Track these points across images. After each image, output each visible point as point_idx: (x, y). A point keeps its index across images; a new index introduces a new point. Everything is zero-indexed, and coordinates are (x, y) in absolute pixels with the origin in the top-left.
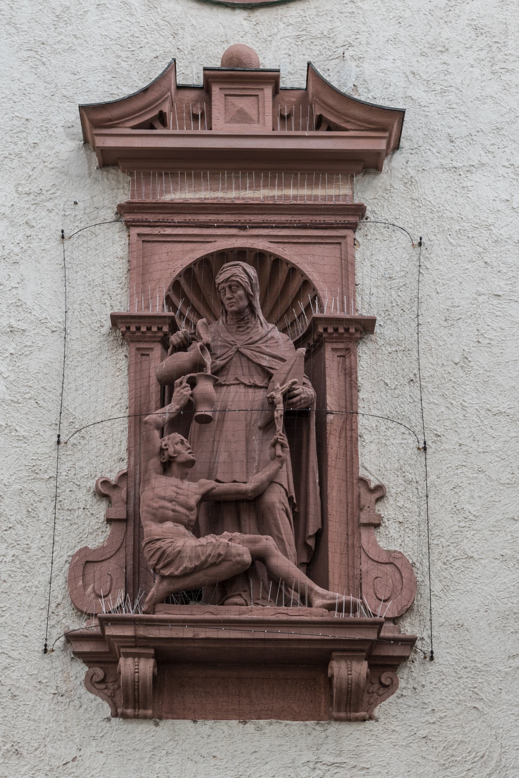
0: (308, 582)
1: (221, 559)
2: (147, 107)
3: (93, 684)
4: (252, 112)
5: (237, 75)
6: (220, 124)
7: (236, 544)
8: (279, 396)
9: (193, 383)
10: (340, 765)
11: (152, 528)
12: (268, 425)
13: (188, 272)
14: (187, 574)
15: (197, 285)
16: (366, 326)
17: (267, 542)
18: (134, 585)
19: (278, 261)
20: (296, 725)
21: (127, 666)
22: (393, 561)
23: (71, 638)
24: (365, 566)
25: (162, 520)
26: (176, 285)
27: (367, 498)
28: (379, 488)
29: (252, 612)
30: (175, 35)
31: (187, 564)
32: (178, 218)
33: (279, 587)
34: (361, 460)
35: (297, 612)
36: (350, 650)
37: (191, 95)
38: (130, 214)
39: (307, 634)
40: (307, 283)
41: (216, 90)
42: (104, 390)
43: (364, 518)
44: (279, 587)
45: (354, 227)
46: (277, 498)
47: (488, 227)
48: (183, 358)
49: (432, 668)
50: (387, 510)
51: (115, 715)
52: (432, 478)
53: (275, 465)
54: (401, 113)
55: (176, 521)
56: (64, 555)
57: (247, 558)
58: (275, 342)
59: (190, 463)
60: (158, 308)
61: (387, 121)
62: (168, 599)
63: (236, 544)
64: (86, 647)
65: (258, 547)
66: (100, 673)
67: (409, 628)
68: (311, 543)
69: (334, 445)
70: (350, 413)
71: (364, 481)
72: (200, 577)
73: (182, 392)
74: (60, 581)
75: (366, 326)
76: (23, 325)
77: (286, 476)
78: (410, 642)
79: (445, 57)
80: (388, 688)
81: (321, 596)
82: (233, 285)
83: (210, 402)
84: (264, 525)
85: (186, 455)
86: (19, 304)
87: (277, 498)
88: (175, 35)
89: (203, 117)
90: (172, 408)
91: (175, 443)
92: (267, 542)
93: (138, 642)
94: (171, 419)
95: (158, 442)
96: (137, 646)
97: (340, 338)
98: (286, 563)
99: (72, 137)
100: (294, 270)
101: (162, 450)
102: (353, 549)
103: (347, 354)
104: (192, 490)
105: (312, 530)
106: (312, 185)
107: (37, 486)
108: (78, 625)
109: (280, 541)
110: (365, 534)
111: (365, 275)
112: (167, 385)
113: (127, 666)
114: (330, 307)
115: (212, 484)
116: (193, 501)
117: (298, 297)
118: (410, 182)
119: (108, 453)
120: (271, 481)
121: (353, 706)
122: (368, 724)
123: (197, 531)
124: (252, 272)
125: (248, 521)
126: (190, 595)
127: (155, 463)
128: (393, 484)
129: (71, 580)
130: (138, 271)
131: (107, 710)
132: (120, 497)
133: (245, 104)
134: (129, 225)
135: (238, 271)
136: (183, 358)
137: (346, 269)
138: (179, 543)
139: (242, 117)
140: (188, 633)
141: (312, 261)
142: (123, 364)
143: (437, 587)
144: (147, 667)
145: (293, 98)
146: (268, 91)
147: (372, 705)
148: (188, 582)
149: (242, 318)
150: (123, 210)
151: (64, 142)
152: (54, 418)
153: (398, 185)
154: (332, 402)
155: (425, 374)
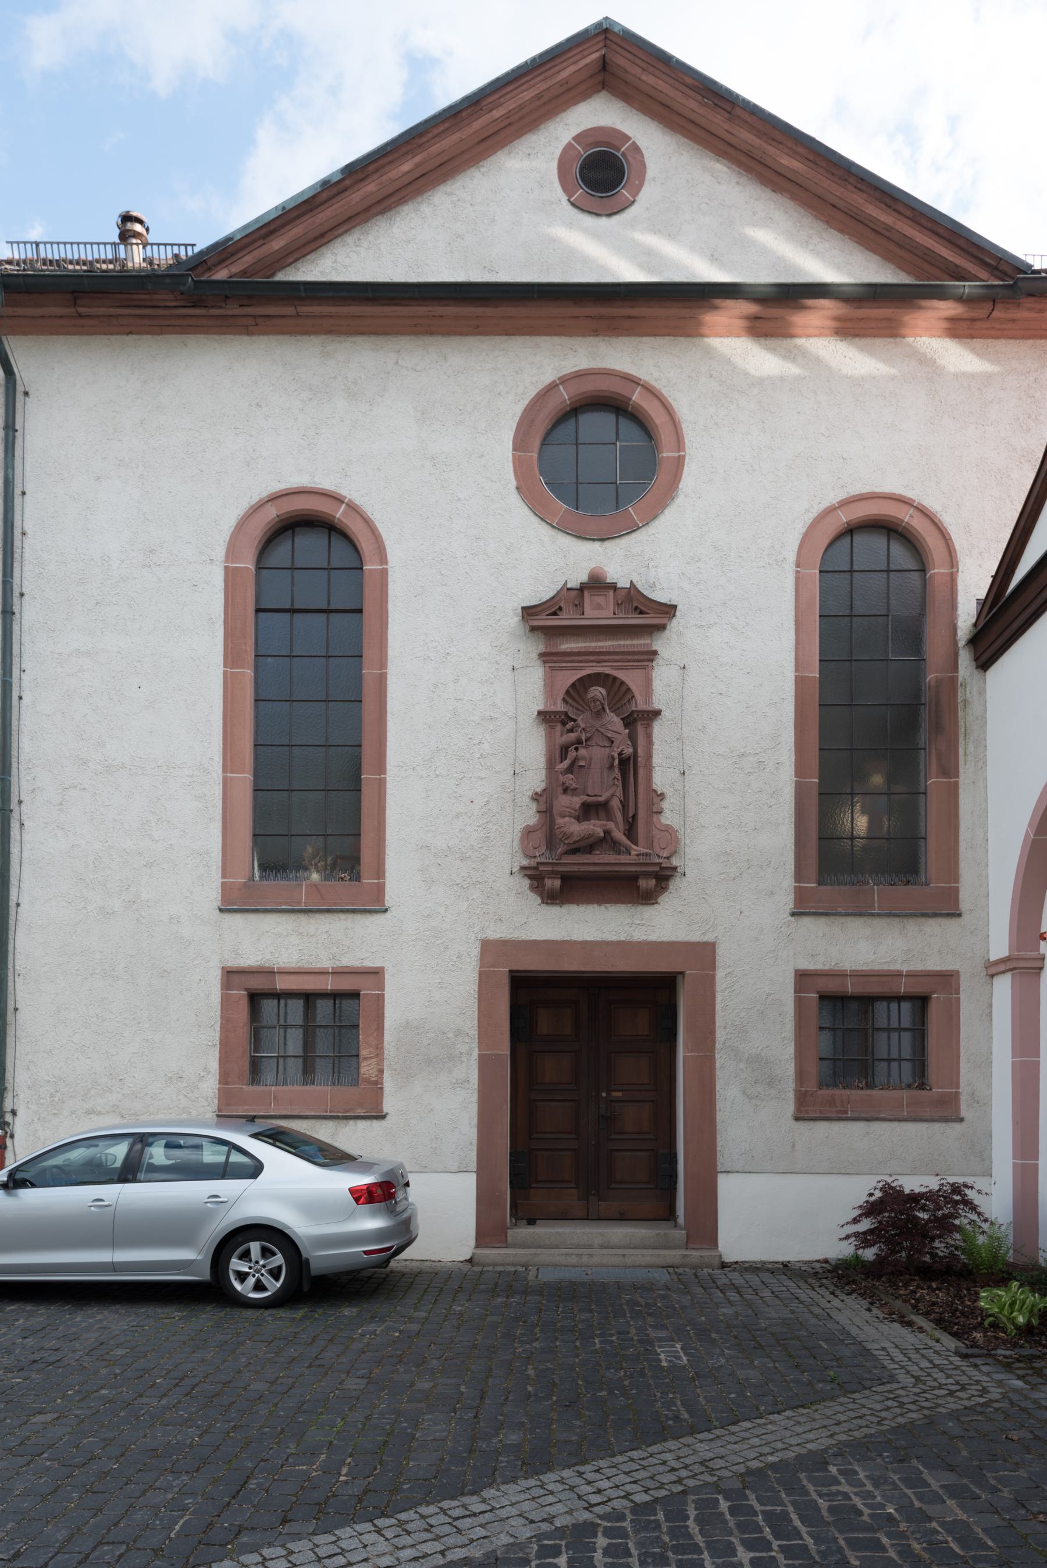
0: (628, 842)
1: (590, 836)
2: (552, 607)
3: (533, 888)
4: (604, 604)
5: (596, 584)
6: (588, 611)
7: (595, 827)
8: (616, 755)
9: (577, 749)
10: (642, 925)
11: (559, 821)
12: (611, 767)
13: (573, 685)
14: (575, 842)
15: (577, 691)
16: (657, 713)
17: (611, 825)
18: (550, 845)
19: (615, 679)
20: (622, 907)
21: (548, 883)
22: (668, 829)
23: (523, 868)
24: (655, 832)
25: (564, 817)
26: (568, 692)
27: (656, 799)
28: (662, 794)
29: (603, 859)
30: (565, 556)
31: (576, 838)
32: (568, 659)
33: (616, 846)
34: (654, 780)
35: (624, 859)
36: (647, 875)
37: (574, 593)
38: (545, 657)
39: (629, 869)
40: (629, 689)
41: (586, 593)
42: (533, 749)
43: (655, 810)
44: (616, 846)
45: (652, 661)
46: (616, 803)
47: (717, 658)
48: (573, 736)
49: (685, 879)
50: (665, 805)
51: (543, 902)
52: (687, 788)
53: (614, 788)
54: (676, 607)
55: (570, 816)
56: (519, 828)
57: (602, 835)
58: (614, 721)
59: (576, 789)
60: (560, 707)
61: (669, 610)
62: (566, 853)
63: (595, 827)
64: (529, 872)
65: (607, 827)
66: (536, 884)
67: (675, 862)
68: (630, 820)
69: (641, 772)
70: (649, 756)
71: (655, 791)
72: (581, 844)
73: (572, 754)
74: (517, 842)
75: (657, 713)
76: (496, 716)
77: (619, 792)
78: (675, 868)
79: (699, 564)
80: (664, 889)
81: (635, 849)
82: (595, 700)
83: (584, 758)
84: (609, 817)
85: (575, 786)
86: (494, 705)
87: (616, 803)
88: (565, 556)
89: (579, 606)
90: (566, 763)
91: (570, 779)
92: (611, 825)
93: (553, 872)
94: (564, 756)
95: (562, 778)
96: (553, 874)
97: (645, 719)
98: (619, 835)
99: (516, 615)
100: (622, 683)
101: (563, 784)
102: (649, 823)
103: (648, 726)
104: (577, 801)
105: (631, 814)
106: (632, 639)
107: (505, 795)
108: (525, 862)
109: (616, 823)
110: (655, 816)
111: (657, 685)
112: (564, 750)
113: (548, 883)
114: (641, 706)
115: (585, 798)
116: (577, 806)
117: (625, 693)
118: (680, 634)
119: (536, 779)
120: (613, 795)
121: (649, 898)
122: (655, 906)
123: (578, 819)
124: (604, 692)
125: (602, 814)
126: (574, 851)
127: (560, 789)
128: (668, 792)
129: (522, 840)
130: (549, 685)
131: (540, 901)
132: (544, 800)
133: (600, 600)
134: (545, 662)
135: (597, 693)
136: (573, 736)
137: (648, 682)
138: (572, 829)
139: (599, 607)
140: (576, 868)
141: (630, 678)
142: (543, 733)
143: (688, 841)
144: (557, 883)
145: (623, 593)
146: (611, 593)
147: (657, 897)
148: (576, 846)
149: (599, 713)
150: (541, 655)
151: (514, 620)
152: (512, 761)
153: (674, 636)
154: (640, 752)
155: (685, 735)
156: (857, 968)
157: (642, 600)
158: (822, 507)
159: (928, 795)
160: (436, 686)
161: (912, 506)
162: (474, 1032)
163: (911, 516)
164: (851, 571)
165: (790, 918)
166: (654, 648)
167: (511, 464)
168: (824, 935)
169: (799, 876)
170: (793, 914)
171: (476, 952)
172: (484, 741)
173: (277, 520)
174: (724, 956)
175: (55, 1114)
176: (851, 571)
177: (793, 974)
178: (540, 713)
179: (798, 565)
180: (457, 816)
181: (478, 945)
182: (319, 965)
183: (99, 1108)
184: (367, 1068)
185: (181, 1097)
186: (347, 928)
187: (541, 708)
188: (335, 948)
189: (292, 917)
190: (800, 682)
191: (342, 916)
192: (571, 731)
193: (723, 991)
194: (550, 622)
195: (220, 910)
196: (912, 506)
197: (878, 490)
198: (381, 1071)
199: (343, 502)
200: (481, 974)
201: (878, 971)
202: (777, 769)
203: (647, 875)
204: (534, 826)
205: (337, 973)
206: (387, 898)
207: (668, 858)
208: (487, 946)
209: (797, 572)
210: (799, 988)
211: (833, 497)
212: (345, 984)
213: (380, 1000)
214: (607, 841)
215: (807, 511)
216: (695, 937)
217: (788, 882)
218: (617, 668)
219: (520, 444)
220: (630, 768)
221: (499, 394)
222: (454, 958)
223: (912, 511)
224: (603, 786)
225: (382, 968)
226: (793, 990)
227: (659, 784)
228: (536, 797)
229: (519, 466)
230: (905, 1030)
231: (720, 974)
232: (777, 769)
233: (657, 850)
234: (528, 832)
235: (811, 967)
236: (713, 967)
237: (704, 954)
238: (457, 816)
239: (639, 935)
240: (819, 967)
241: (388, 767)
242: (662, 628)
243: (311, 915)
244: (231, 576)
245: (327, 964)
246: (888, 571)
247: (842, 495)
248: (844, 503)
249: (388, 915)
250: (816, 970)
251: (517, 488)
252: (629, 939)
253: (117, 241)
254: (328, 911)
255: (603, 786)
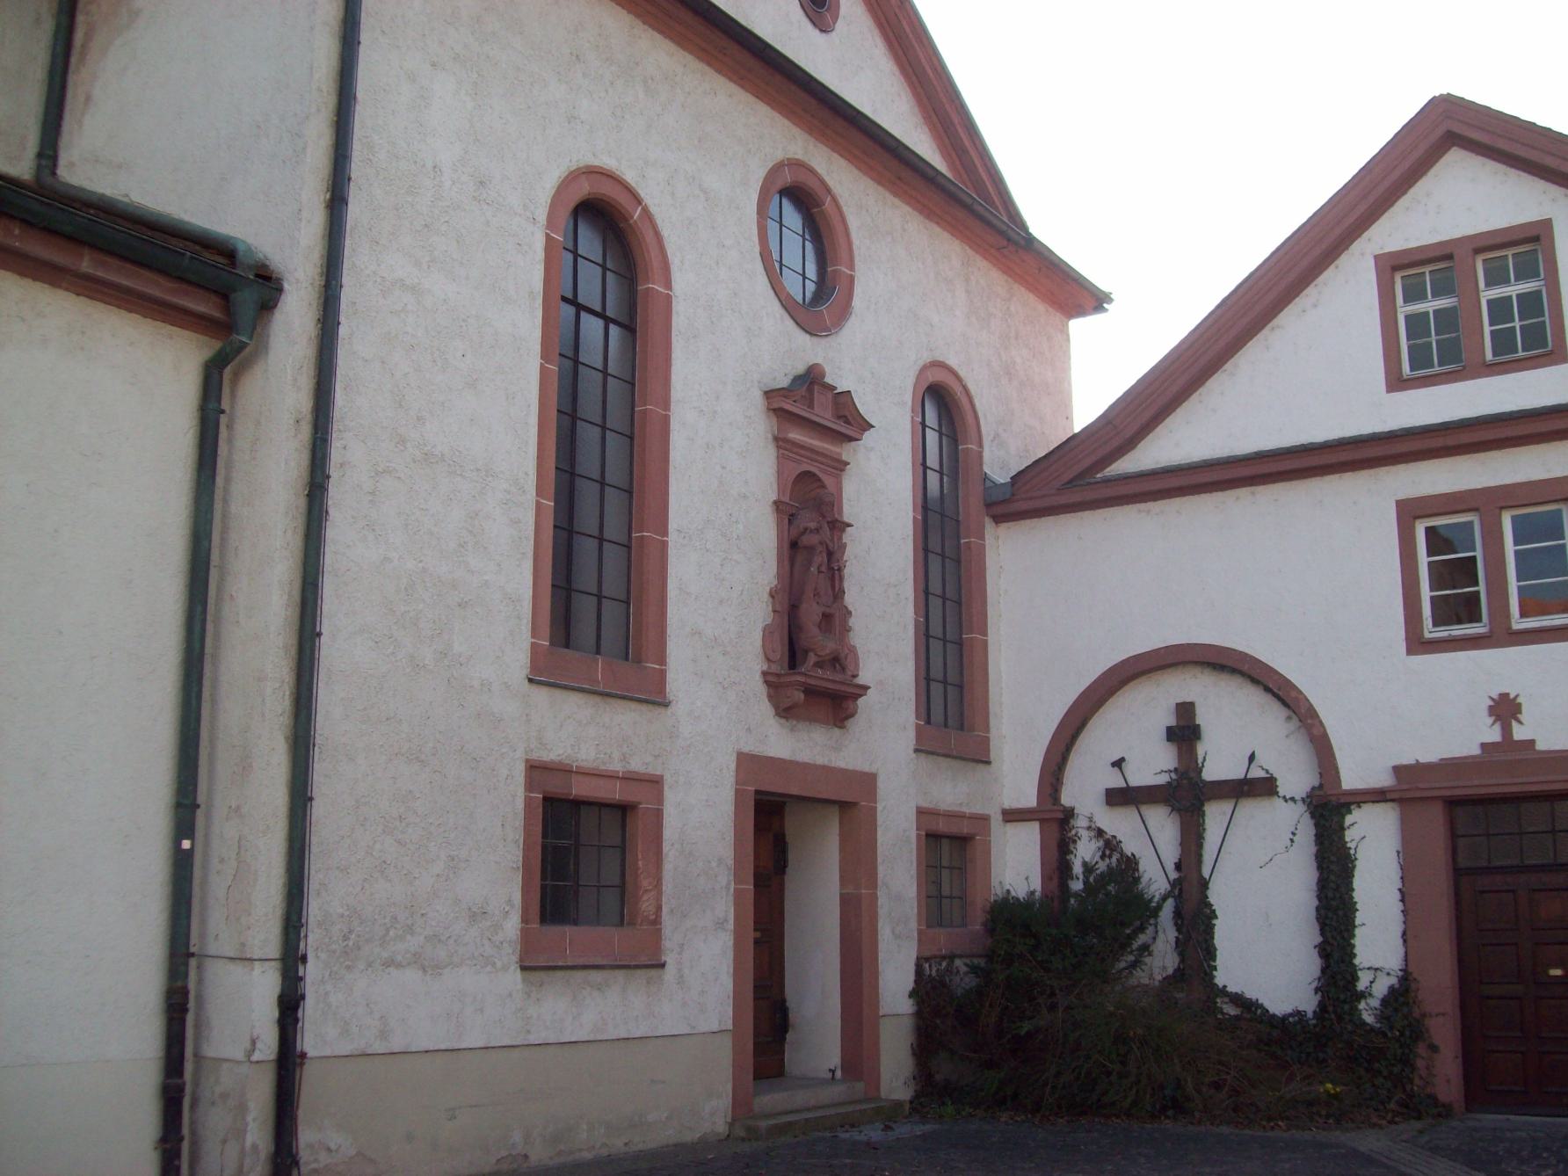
64: (771, 678)
162: (731, 862)
164: (1553, 831)
166: (844, 458)
175: (348, 967)
176: (1553, 831)
181: (734, 757)
182: (611, 768)
183: (399, 958)
184: (646, 905)
185: (486, 942)
191: (633, 705)
195: (530, 680)
198: (659, 908)
200: (737, 791)
212: (616, 793)
213: (659, 814)
218: (825, 472)
242: (851, 439)
245: (617, 766)
253: (1519, 733)
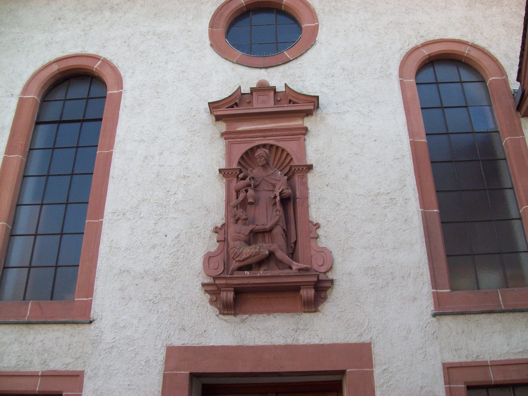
5: (263, 88)
8: (278, 194)
19: (278, 147)
32: (242, 136)
33: (280, 263)
36: (307, 285)
38: (225, 135)
41: (254, 94)
43: (312, 236)
44: (280, 263)
50: (320, 232)
51: (220, 313)
61: (315, 100)
63: (262, 248)
64: (209, 288)
67: (330, 276)
68: (293, 245)
71: (311, 222)
79: (333, 78)
81: (296, 266)
93: (227, 286)
98: (281, 255)
100: (283, 150)
105: (293, 240)
108: (208, 280)
119: (218, 217)
137: (303, 149)
141: (289, 146)
144: (231, 295)
156: (496, 359)
157: (293, 95)
158: (411, 47)
159: (523, 220)
160: (146, 157)
161: (468, 45)
163: (469, 50)
165: (433, 319)
167: (208, 34)
168: (463, 332)
169: (435, 284)
170: (435, 315)
171: (161, 356)
172: (178, 192)
173: (58, 72)
174: (379, 354)
177: (441, 367)
178: (220, 171)
179: (400, 76)
180: (154, 247)
181: (164, 351)
182: (32, 369)
186: (58, 338)
187: (223, 166)
188: (46, 355)
189: (17, 328)
190: (414, 145)
191: (55, 327)
192: (244, 179)
193: (382, 386)
194: (229, 111)
196: (468, 45)
197: (445, 38)
199: (100, 59)
201: (514, 360)
202: (406, 203)
203: (307, 285)
204: (216, 252)
205: (46, 375)
206: (92, 312)
207: (325, 273)
208: (171, 351)
209: (400, 80)
210: (448, 380)
211: (416, 42)
214: (270, 258)
215: (401, 49)
216: (353, 339)
217: (426, 289)
219: (212, 25)
220: (290, 203)
221: (202, 3)
222: (143, 363)
223: (469, 48)
224: (266, 216)
225: (83, 372)
226: (443, 382)
227: (314, 217)
228: (216, 230)
229: (212, 35)
230: (318, 278)
231: (377, 371)
232: (406, 203)
233: (315, 267)
234: (209, 258)
235: (456, 360)
236: (370, 364)
237: (362, 352)
238: (154, 247)
239: (304, 339)
240: (463, 359)
241: (105, 213)
243: (31, 326)
244: (21, 102)
246: (442, 108)
247: (422, 41)
248: (424, 45)
249: (92, 326)
250: (461, 363)
251: (211, 45)
252: (295, 343)
254: (44, 323)
255: (266, 216)
